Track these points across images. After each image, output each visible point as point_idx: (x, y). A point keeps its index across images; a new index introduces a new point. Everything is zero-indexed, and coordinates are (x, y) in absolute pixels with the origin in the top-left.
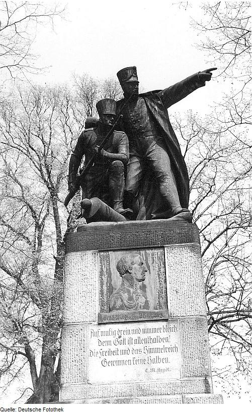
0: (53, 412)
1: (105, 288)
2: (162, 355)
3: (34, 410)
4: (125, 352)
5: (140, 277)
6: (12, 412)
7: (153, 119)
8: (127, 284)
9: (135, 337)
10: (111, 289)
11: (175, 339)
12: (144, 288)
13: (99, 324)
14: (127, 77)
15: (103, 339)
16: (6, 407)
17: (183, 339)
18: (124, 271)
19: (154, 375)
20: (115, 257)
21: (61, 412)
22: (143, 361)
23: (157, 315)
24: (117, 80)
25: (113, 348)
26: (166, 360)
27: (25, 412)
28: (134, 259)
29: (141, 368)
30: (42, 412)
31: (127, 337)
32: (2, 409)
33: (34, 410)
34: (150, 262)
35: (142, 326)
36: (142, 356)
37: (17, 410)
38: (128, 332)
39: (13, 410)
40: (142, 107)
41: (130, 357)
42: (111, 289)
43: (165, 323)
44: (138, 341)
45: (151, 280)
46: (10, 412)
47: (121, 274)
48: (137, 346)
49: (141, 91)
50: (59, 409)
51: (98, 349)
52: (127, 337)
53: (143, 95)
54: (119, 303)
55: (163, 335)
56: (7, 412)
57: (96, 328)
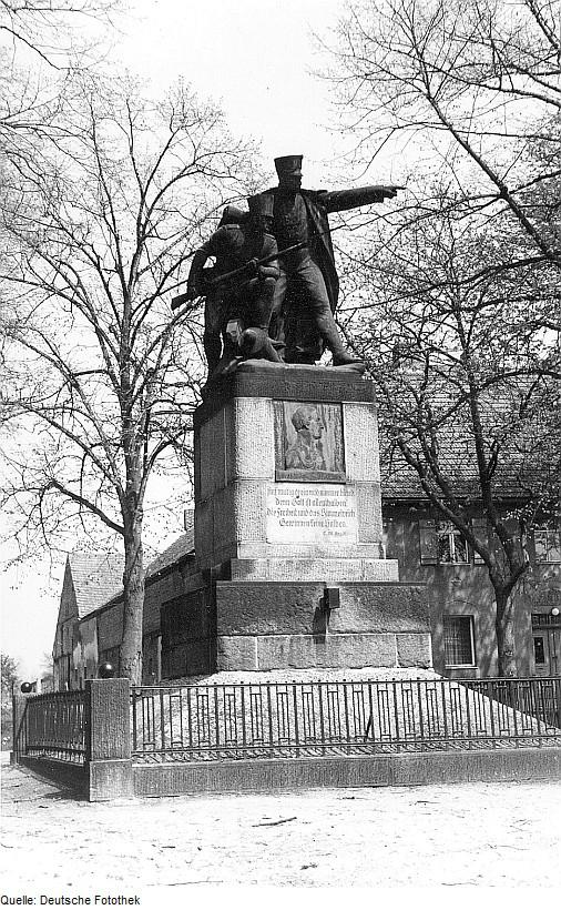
0: (117, 907)
1: (279, 442)
2: (340, 519)
3: (75, 901)
4: (303, 513)
5: (317, 434)
6: (27, 907)
7: (312, 226)
8: (303, 441)
9: (313, 498)
10: (286, 445)
11: (351, 503)
12: (320, 446)
13: (276, 482)
14: (288, 167)
15: (281, 498)
16: (13, 895)
17: (360, 504)
18: (300, 425)
19: (332, 538)
20: (291, 408)
21: (134, 907)
22: (321, 524)
23: (335, 477)
24: (274, 169)
25: (291, 508)
26: (343, 524)
27: (55, 907)
28: (311, 413)
29: (319, 530)
30: (92, 906)
31: (305, 498)
32: (4, 900)
33: (75, 901)
34: (327, 419)
35: (320, 488)
36: (320, 519)
37: (37, 901)
38: (306, 493)
39: (29, 901)
40: (300, 209)
41: (309, 518)
42: (286, 445)
43: (342, 486)
44: (316, 503)
45: (328, 439)
46: (22, 907)
47: (297, 429)
48: (315, 508)
49: (306, 185)
50: (131, 899)
51: (275, 508)
52: (305, 498)
53: (305, 193)
54: (297, 461)
55: (341, 499)
56: (16, 906)
57: (273, 486)
